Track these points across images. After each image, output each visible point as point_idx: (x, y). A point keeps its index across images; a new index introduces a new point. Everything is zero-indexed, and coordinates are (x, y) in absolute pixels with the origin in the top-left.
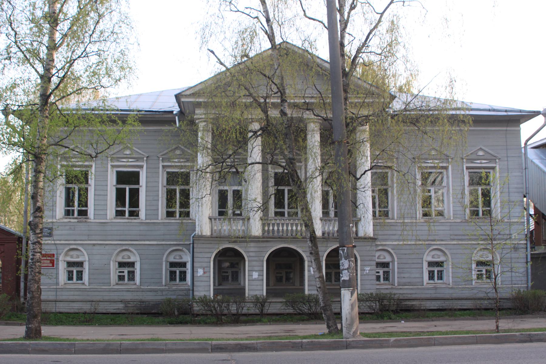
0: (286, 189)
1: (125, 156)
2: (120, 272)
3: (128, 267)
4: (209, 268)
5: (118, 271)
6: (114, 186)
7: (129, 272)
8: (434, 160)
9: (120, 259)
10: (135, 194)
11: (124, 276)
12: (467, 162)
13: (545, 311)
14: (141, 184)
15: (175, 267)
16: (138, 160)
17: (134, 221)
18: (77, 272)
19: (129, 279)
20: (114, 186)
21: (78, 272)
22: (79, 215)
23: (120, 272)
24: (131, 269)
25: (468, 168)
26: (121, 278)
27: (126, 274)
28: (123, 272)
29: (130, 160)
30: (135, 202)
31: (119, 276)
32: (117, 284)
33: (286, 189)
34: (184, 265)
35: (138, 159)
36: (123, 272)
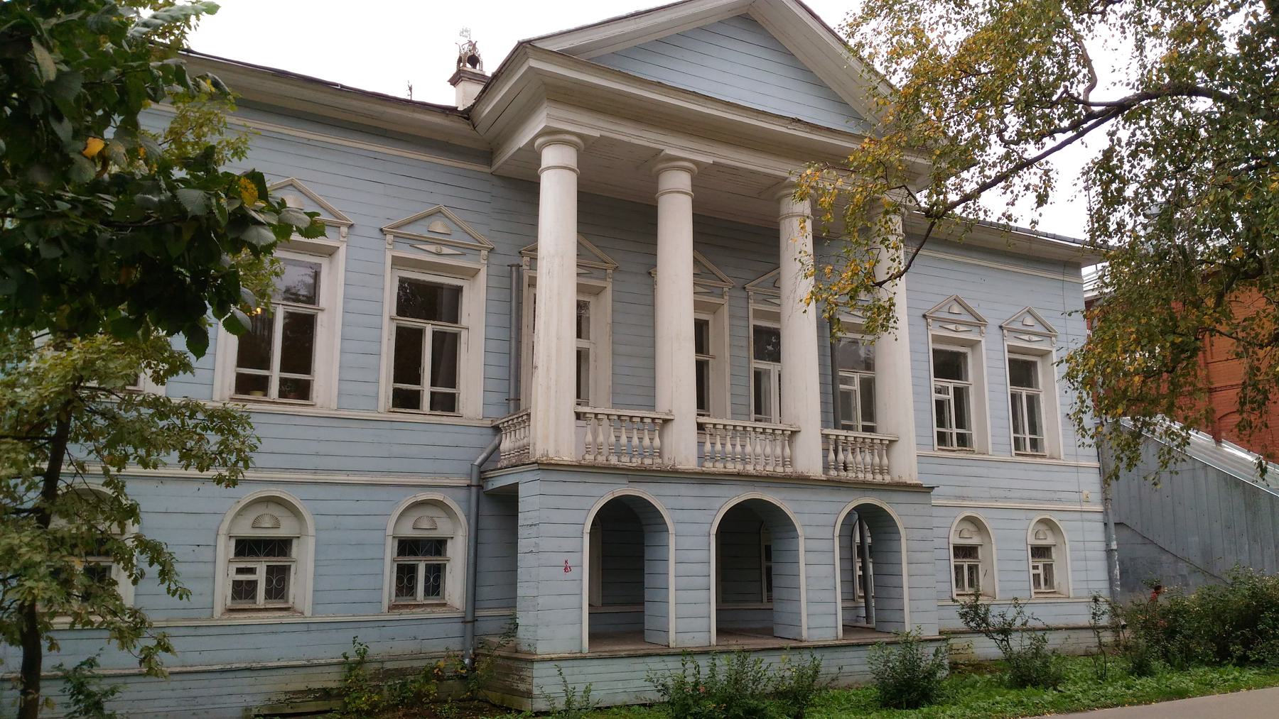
0: (429, 329)
1: (1025, 328)
2: (239, 571)
3: (267, 555)
4: (578, 555)
5: (234, 566)
6: (322, 310)
7: (270, 570)
8: (958, 326)
9: (246, 530)
10: (447, 348)
11: (253, 584)
12: (756, 301)
13: (3, 680)
14: (465, 319)
15: (413, 552)
16: (464, 254)
17: (294, 407)
18: (428, 568)
19: (269, 594)
20: (322, 310)
21: (970, 568)
22: (282, 394)
23: (239, 571)
24: (435, 560)
25: (397, 262)
26: (243, 590)
27: (261, 576)
28: (252, 571)
29: (446, 250)
30: (446, 370)
31: (237, 584)
32: (232, 610)
33: (429, 329)
34: (438, 546)
35: (465, 249)
36: (252, 571)
